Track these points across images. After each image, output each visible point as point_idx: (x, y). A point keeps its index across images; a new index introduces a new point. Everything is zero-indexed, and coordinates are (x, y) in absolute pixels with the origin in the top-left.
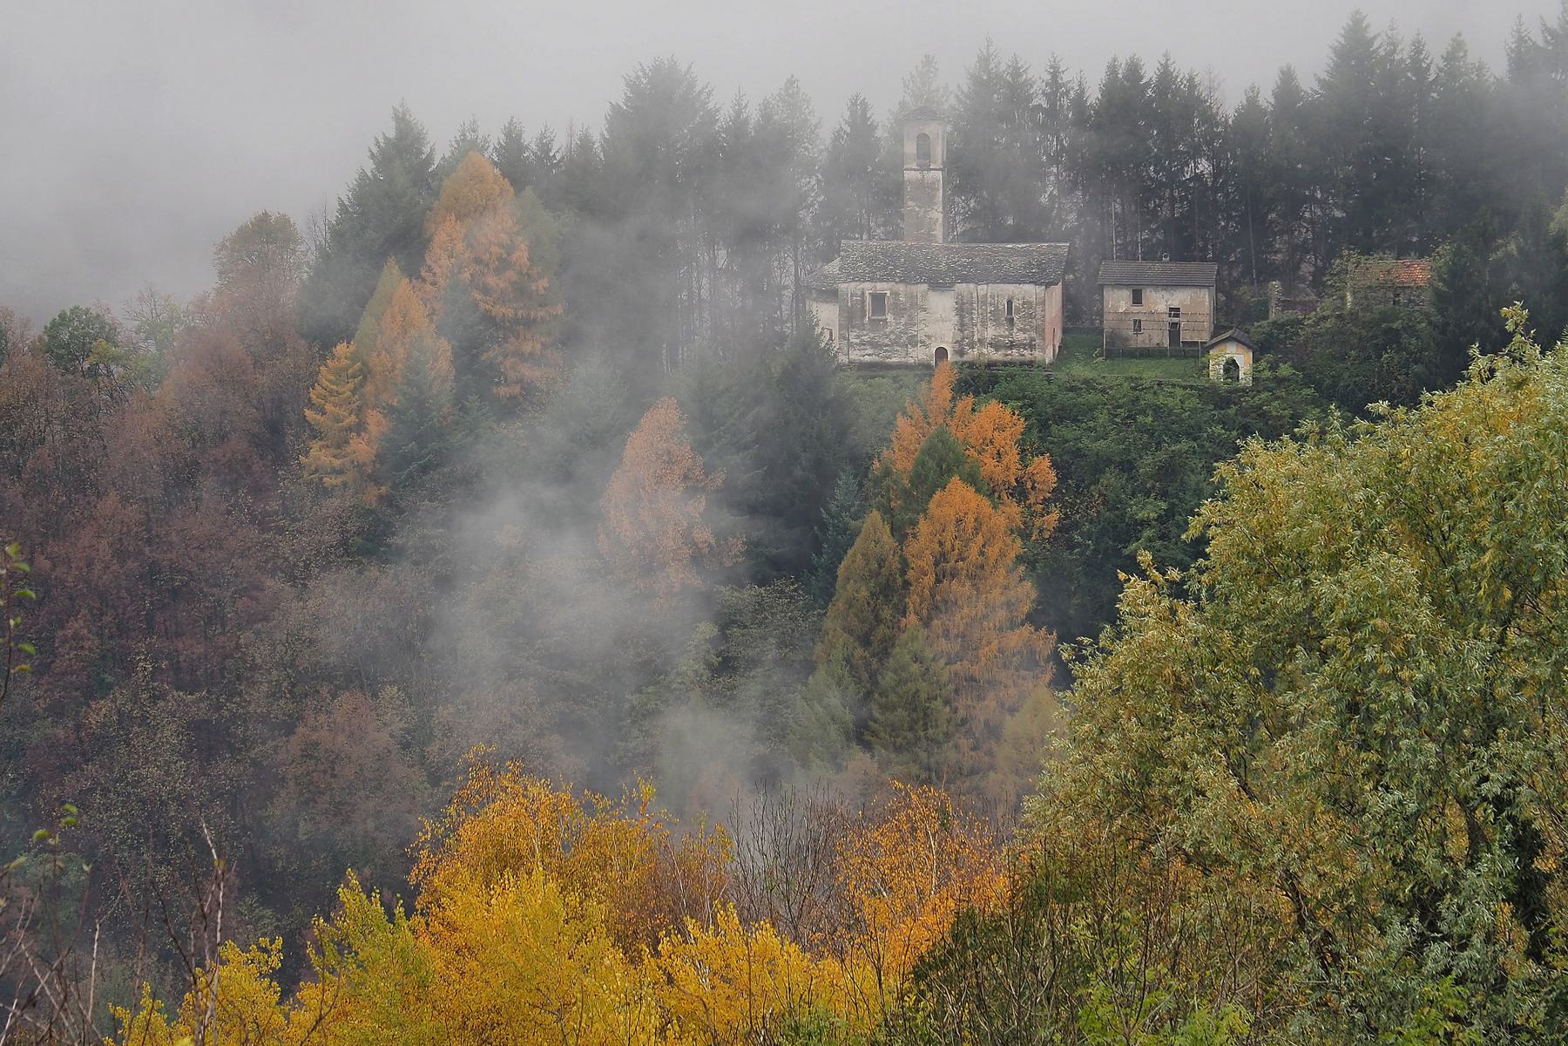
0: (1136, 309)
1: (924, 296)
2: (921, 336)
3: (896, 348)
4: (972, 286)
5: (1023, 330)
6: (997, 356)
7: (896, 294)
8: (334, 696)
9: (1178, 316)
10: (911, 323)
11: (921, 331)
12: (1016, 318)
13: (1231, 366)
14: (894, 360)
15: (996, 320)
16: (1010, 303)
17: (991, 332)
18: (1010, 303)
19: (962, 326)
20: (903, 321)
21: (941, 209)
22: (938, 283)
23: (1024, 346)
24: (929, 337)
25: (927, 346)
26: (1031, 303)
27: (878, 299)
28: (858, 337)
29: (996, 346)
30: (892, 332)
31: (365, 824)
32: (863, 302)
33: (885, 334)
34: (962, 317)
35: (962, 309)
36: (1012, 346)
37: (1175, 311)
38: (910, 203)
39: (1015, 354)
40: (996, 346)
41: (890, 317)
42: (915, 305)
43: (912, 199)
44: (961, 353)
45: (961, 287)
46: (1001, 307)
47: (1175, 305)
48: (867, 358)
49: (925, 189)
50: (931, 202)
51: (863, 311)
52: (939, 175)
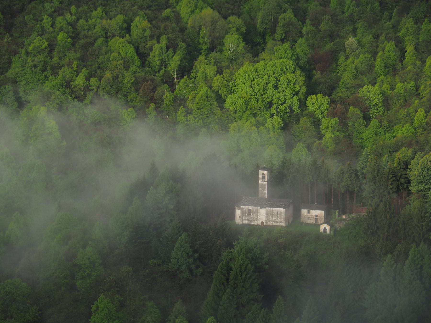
0: (308, 214)
1: (259, 210)
2: (258, 219)
3: (253, 221)
4: (269, 208)
5: (280, 219)
6: (275, 224)
7: (253, 209)
8: (219, 46)
9: (317, 217)
10: (256, 216)
11: (259, 218)
12: (279, 216)
13: (325, 229)
14: (252, 223)
15: (275, 216)
16: (278, 212)
17: (273, 219)
18: (278, 212)
19: (267, 217)
20: (254, 215)
21: (267, 190)
22: (263, 207)
23: (280, 222)
24: (260, 219)
25: (259, 221)
26: (282, 213)
27: (249, 210)
28: (245, 218)
29: (275, 222)
30: (252, 217)
31: (168, 38)
32: (246, 210)
33: (250, 218)
34: (267, 215)
35: (267, 213)
36: (278, 222)
37: (317, 216)
38: (260, 189)
39: (278, 224)
40: (275, 222)
41: (252, 214)
42: (257, 212)
43: (260, 188)
44: (267, 223)
45: (267, 208)
46: (276, 213)
47: (317, 214)
48: (246, 223)
49: (263, 185)
50: (264, 189)
51: (246, 212)
52: (267, 183)
